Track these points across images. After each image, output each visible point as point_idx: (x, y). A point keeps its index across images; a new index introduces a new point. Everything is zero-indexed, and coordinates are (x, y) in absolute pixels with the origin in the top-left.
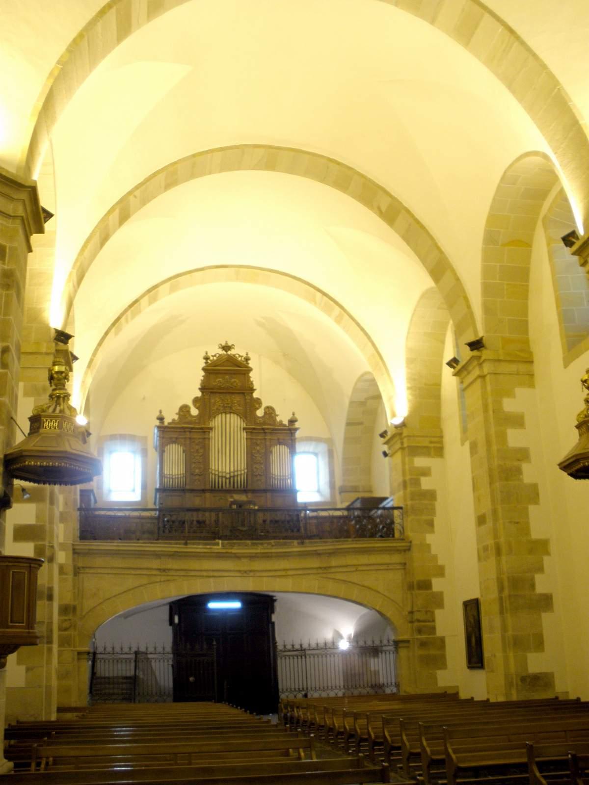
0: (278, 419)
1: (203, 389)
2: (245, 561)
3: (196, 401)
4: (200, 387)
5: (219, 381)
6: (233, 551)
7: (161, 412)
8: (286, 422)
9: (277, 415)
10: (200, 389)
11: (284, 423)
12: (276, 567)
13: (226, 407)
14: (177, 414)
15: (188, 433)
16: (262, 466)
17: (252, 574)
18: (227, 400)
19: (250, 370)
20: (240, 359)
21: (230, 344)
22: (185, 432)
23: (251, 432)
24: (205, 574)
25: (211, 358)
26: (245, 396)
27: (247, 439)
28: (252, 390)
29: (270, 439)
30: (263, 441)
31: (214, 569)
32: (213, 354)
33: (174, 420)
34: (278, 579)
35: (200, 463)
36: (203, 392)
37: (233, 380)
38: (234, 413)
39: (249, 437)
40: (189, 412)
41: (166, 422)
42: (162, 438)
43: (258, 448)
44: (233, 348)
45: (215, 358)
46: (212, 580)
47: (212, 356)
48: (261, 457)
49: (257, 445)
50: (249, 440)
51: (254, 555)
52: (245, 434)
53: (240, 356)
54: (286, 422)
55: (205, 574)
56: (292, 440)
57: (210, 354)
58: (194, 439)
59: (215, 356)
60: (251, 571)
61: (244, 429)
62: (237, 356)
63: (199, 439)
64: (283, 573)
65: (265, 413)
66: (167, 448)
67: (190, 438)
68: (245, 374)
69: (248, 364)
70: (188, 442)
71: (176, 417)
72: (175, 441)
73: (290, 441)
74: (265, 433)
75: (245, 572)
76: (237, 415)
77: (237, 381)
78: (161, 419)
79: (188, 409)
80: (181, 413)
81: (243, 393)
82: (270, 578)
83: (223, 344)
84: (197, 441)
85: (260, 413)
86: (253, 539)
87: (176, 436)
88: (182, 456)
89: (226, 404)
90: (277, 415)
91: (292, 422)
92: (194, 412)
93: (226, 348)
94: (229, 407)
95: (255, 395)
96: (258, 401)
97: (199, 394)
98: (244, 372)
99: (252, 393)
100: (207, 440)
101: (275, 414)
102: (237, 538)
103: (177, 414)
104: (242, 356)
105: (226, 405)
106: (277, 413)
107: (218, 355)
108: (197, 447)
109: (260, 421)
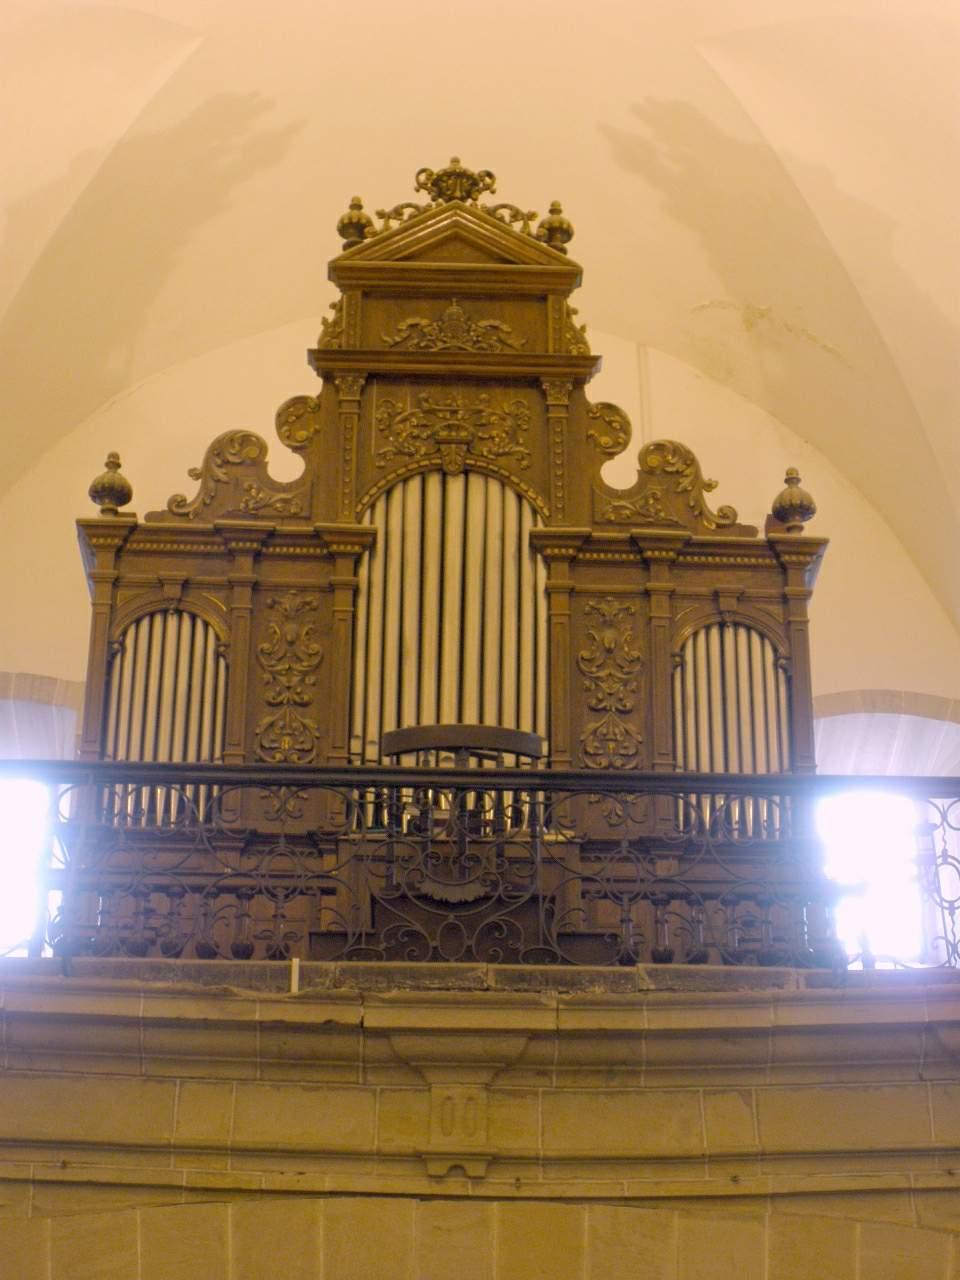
0: (713, 502)
1: (325, 360)
2: (456, 1089)
3: (293, 415)
4: (315, 346)
5: (412, 326)
6: (375, 1018)
7: (114, 463)
8: (754, 514)
9: (710, 487)
10: (311, 352)
11: (742, 520)
12: (484, 285)
13: (448, 442)
14: (194, 474)
15: (246, 562)
16: (632, 728)
17: (500, 1182)
18: (455, 412)
19: (572, 277)
20: (517, 226)
21: (473, 167)
22: (231, 554)
23: (573, 561)
24: (185, 1172)
25: (378, 224)
26: (544, 394)
27: (548, 593)
28: (584, 366)
29: (672, 594)
30: (635, 606)
31: (243, 1139)
32: (388, 209)
33: (178, 502)
34: (677, 1221)
35: (304, 705)
36: (327, 377)
37: (484, 323)
38: (487, 474)
39: (564, 580)
40: (258, 463)
41: (140, 507)
42: (108, 585)
43: (608, 636)
44: (488, 187)
45: (395, 224)
46: (229, 1212)
47: (381, 215)
48: (625, 683)
49: (608, 624)
50: (562, 600)
51: (513, 1047)
52: (542, 572)
53: (516, 215)
54: (754, 514)
55: (185, 1172)
56: (785, 599)
57: (369, 211)
58: (278, 588)
59: (397, 213)
60: (495, 1160)
61: (538, 544)
62: (506, 213)
63: (303, 589)
64: (715, 1181)
65: (647, 473)
66: (137, 639)
67: (256, 587)
68: (543, 299)
69: (564, 251)
70: (243, 598)
71: (191, 490)
72: (177, 604)
73: (776, 609)
74: (646, 563)
75: (457, 1164)
76: (504, 483)
77: (505, 328)
78: (113, 493)
79: (253, 452)
80: (220, 473)
81: (534, 382)
82: (625, 1212)
83: (439, 166)
84: (288, 602)
85: (620, 473)
86: (512, 956)
87: (182, 574)
88: (211, 675)
89: (449, 427)
90: (710, 487)
91: (789, 512)
92: (285, 465)
93: (455, 161)
94: (460, 442)
95: (596, 391)
96: (612, 423)
97: (312, 385)
98: (537, 287)
99: (579, 383)
100: (342, 599)
101: (697, 475)
102: (409, 945)
103: (194, 474)
104: (531, 216)
105: (444, 434)
106: (707, 474)
107: (407, 212)
108: (291, 628)
109: (616, 509)
